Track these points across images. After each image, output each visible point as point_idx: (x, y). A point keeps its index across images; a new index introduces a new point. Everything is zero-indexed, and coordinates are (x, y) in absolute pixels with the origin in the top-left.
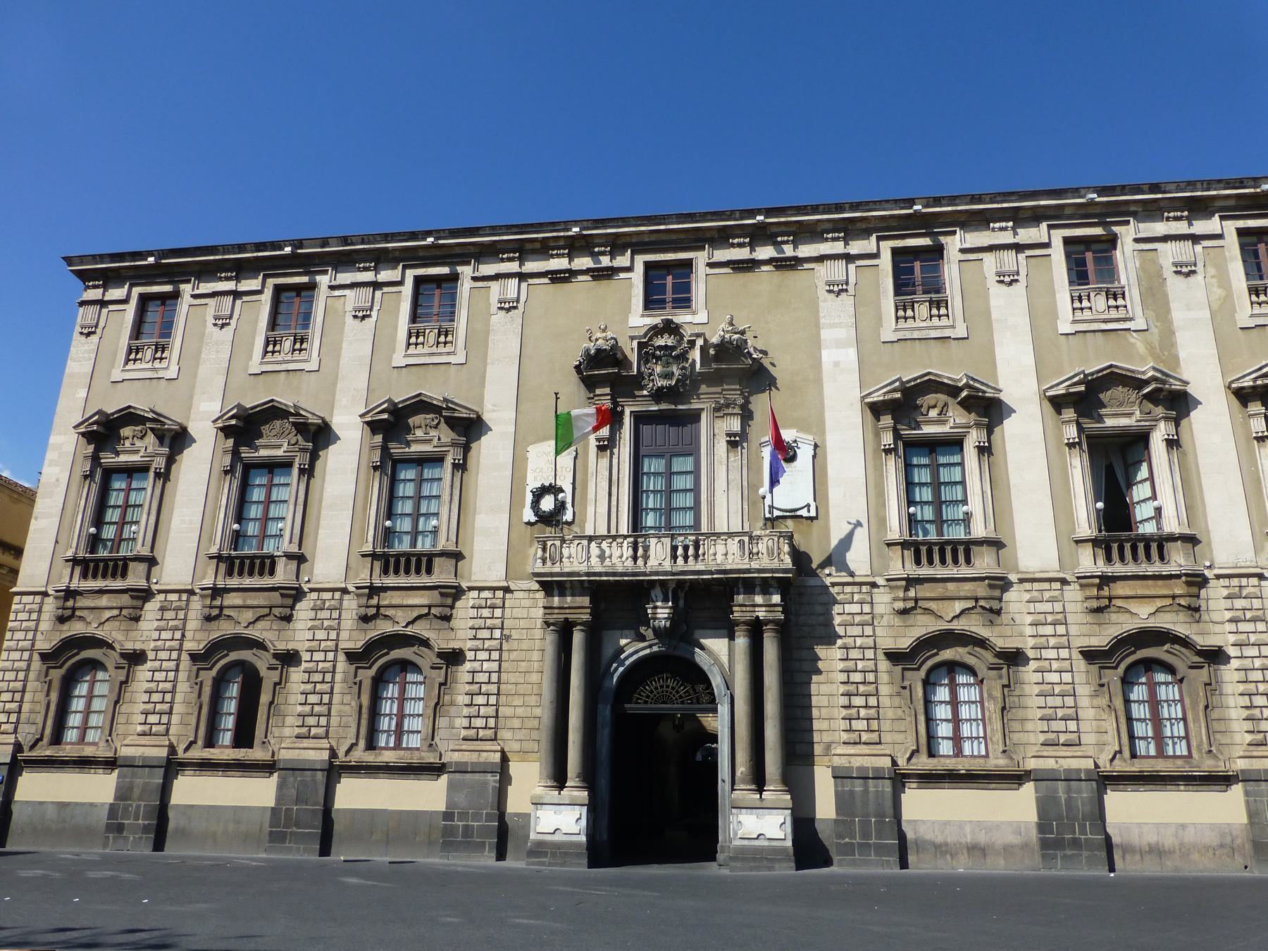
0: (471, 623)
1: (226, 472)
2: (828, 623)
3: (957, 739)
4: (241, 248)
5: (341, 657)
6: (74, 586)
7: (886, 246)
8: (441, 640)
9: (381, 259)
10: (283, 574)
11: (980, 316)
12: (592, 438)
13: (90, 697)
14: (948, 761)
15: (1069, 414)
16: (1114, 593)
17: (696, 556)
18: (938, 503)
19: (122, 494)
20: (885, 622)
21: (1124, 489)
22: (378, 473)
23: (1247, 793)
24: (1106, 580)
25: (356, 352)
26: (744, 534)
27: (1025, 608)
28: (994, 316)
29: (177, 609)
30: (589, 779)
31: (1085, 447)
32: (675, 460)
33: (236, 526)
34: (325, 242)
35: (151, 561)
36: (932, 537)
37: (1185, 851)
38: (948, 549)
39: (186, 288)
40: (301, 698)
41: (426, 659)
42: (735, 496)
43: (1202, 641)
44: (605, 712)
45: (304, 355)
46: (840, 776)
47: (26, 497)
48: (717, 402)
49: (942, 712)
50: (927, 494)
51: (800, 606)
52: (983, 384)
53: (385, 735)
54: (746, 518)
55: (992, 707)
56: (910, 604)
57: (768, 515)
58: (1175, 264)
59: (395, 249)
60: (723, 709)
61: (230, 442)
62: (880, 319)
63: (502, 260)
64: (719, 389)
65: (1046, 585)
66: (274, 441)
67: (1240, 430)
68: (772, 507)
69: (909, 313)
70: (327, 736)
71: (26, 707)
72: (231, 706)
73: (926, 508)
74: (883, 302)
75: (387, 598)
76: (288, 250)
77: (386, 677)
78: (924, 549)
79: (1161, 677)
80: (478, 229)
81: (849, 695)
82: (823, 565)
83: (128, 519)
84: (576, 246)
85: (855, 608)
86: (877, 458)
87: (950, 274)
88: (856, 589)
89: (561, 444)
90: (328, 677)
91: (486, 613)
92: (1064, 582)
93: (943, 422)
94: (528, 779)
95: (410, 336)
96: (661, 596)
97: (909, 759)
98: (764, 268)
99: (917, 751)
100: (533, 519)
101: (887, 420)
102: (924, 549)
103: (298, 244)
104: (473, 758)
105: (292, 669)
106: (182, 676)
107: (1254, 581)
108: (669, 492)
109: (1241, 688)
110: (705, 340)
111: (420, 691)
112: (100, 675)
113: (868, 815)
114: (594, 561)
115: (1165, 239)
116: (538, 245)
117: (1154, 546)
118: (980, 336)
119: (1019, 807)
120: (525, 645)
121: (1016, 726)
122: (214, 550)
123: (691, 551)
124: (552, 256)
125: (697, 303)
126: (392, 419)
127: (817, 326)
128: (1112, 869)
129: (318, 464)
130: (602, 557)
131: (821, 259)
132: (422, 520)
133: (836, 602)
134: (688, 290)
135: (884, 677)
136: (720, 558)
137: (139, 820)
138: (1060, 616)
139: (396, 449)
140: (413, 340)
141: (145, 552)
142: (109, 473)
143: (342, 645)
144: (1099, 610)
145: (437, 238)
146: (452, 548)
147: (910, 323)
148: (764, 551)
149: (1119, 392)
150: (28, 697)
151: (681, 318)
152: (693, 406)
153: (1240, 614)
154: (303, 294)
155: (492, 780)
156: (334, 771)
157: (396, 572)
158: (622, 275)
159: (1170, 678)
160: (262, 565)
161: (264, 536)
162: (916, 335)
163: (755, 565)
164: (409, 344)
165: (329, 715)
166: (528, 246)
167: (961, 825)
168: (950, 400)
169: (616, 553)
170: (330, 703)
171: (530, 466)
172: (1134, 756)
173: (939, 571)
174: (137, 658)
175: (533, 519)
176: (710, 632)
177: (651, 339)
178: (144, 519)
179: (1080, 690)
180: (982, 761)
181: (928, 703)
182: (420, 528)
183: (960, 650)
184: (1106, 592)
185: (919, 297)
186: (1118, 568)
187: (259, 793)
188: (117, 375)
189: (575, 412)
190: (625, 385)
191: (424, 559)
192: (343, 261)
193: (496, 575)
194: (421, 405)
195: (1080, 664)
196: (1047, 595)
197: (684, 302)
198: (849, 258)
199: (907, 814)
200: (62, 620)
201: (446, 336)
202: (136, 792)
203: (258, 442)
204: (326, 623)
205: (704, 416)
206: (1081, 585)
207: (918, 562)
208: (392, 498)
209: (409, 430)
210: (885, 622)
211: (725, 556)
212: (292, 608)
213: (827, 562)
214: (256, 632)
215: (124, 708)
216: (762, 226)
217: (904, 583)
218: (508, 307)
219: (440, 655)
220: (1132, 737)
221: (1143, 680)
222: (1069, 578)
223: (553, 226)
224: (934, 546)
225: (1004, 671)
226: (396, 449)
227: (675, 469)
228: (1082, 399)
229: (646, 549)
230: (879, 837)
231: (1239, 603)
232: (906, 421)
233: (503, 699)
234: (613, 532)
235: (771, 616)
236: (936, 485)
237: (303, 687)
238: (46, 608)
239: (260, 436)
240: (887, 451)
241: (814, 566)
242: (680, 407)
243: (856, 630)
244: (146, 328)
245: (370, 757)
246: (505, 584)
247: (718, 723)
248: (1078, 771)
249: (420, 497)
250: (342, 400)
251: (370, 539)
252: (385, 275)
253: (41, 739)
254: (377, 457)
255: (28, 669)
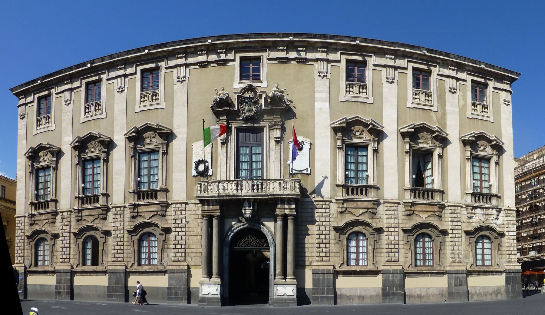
0: (173, 217)
1: (77, 164)
2: (313, 216)
3: (357, 259)
4: (71, 68)
5: (126, 232)
6: (33, 213)
7: (344, 57)
8: (163, 224)
9: (127, 63)
10: (102, 202)
11: (378, 95)
12: (219, 139)
13: (44, 250)
14: (353, 267)
15: (407, 140)
16: (415, 209)
17: (262, 189)
18: (357, 171)
19: (43, 178)
20: (334, 216)
21: (422, 171)
22: (133, 159)
23: (448, 278)
24: (413, 204)
25: (120, 107)
26: (281, 180)
27: (384, 212)
28: (384, 96)
29: (67, 218)
30: (221, 275)
31: (411, 154)
32: (253, 148)
33: (83, 185)
34: (103, 59)
35: (56, 201)
36: (354, 184)
37: (428, 296)
38: (359, 189)
39: (53, 91)
40: (113, 248)
41: (157, 232)
42: (278, 164)
43: (441, 228)
44: (226, 250)
45: (100, 112)
46: (314, 273)
47: (13, 183)
48: (271, 123)
49: (353, 250)
50: (352, 167)
51: (302, 209)
52: (377, 124)
53: (144, 260)
54: (282, 173)
55: (370, 248)
56: (344, 210)
57: (291, 172)
58: (450, 88)
59: (132, 58)
60: (272, 249)
61: (77, 152)
62: (340, 91)
63: (178, 58)
64: (272, 117)
65: (393, 205)
66: (93, 150)
67: (462, 154)
68: (292, 169)
69: (351, 89)
70: (123, 261)
71: (26, 255)
72: (89, 251)
73: (352, 172)
74: (341, 83)
75: (141, 209)
76: (89, 65)
77: (143, 239)
78: (350, 188)
79: (427, 239)
80: (166, 43)
81: (319, 243)
82: (312, 194)
83: (46, 187)
84: (210, 49)
85: (323, 211)
86: (335, 151)
87: (368, 74)
88: (324, 203)
89: (206, 142)
90: (122, 240)
91: (179, 213)
92: (399, 204)
93: (361, 138)
94: (198, 276)
95: (85, 110)
96: (248, 205)
97: (340, 267)
98: (292, 62)
99: (343, 264)
100: (196, 174)
101: (340, 135)
102: (350, 188)
103: (92, 62)
104: (177, 268)
105: (109, 237)
106: (72, 242)
107: (459, 208)
108: (251, 162)
109: (451, 243)
110: (266, 95)
111: (156, 244)
112: (46, 243)
113: (324, 286)
114: (221, 191)
115: (448, 77)
116: (193, 50)
117: (430, 193)
118: (377, 104)
119: (375, 283)
120: (195, 225)
121: (378, 255)
122: (76, 195)
123: (260, 187)
124: (199, 55)
125: (263, 77)
126: (137, 135)
127: (314, 91)
128: (405, 303)
129: (110, 157)
130: (224, 189)
131: (316, 60)
132: (152, 176)
133: (316, 208)
134: (259, 71)
135: (333, 237)
136: (271, 190)
137: (65, 290)
138: (396, 216)
139: (140, 148)
140: (142, 99)
141: (54, 198)
142: (38, 170)
143: (125, 228)
144: (410, 215)
145: (149, 50)
146: (164, 187)
147: (351, 94)
148: (289, 187)
149: (425, 134)
150: (26, 251)
151: (256, 84)
152: (261, 125)
153: (454, 219)
154: (97, 84)
155: (185, 276)
156: (127, 273)
157: (87, 203)
158: (230, 63)
159: (430, 240)
160: (94, 199)
161: (93, 188)
162: (353, 99)
163: (285, 193)
164: (141, 101)
165: (123, 253)
166: (189, 50)
167: (356, 289)
168: (364, 129)
169: (230, 188)
170: (123, 249)
171: (194, 152)
172: (416, 266)
173: (355, 197)
174: (56, 236)
175: (196, 174)
176: (267, 219)
177: (243, 94)
178: (51, 185)
179: (400, 243)
180: (365, 267)
181: (348, 246)
182: (151, 180)
183: (361, 227)
184: (412, 209)
185: (356, 83)
186: (417, 200)
187: (103, 281)
188: (35, 132)
189: (211, 128)
190: (232, 115)
191: (154, 193)
192: (111, 67)
193: (182, 198)
194: (148, 128)
195: (401, 234)
196: (393, 208)
197: (257, 77)
198: (328, 61)
199: (338, 286)
200: (31, 225)
201: (156, 96)
202: (63, 281)
203: (87, 151)
204: (119, 220)
205: (265, 129)
206: (405, 206)
207: (348, 194)
208: (139, 168)
209: (144, 139)
210: (334, 216)
211: (273, 189)
212: (106, 215)
213: (313, 192)
214: (94, 224)
215: (55, 254)
216: (292, 42)
217: (342, 201)
218: (181, 80)
219: (162, 230)
220: (416, 259)
221: (421, 240)
222: (401, 202)
223: (199, 40)
224: (354, 187)
225: (376, 235)
226: (140, 148)
227: (253, 152)
228: (412, 135)
229: (242, 186)
230: (328, 293)
231: (454, 215)
232: (347, 136)
233: (187, 246)
234: (228, 179)
235: (291, 213)
236: (357, 163)
237: (113, 244)
238: (26, 221)
239: (87, 148)
240: (339, 148)
241: (308, 194)
242: (256, 125)
243: (324, 219)
244: (42, 111)
245: (139, 268)
246: (186, 201)
247: (270, 254)
248: (397, 270)
249: (150, 168)
250: (117, 129)
251: (133, 186)
252: (129, 71)
253: (31, 265)
254: (132, 152)
255: (24, 242)
